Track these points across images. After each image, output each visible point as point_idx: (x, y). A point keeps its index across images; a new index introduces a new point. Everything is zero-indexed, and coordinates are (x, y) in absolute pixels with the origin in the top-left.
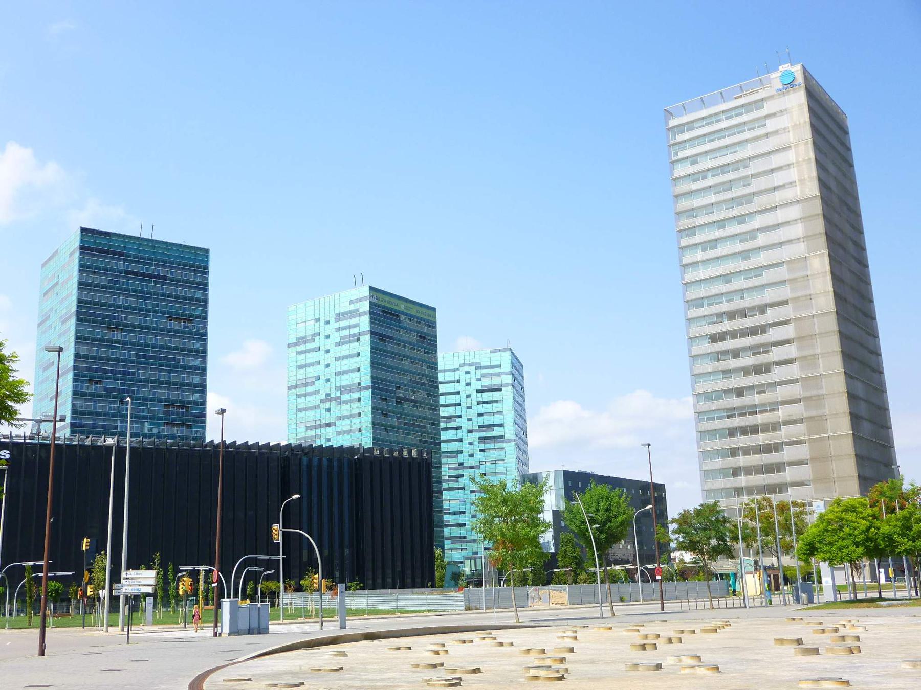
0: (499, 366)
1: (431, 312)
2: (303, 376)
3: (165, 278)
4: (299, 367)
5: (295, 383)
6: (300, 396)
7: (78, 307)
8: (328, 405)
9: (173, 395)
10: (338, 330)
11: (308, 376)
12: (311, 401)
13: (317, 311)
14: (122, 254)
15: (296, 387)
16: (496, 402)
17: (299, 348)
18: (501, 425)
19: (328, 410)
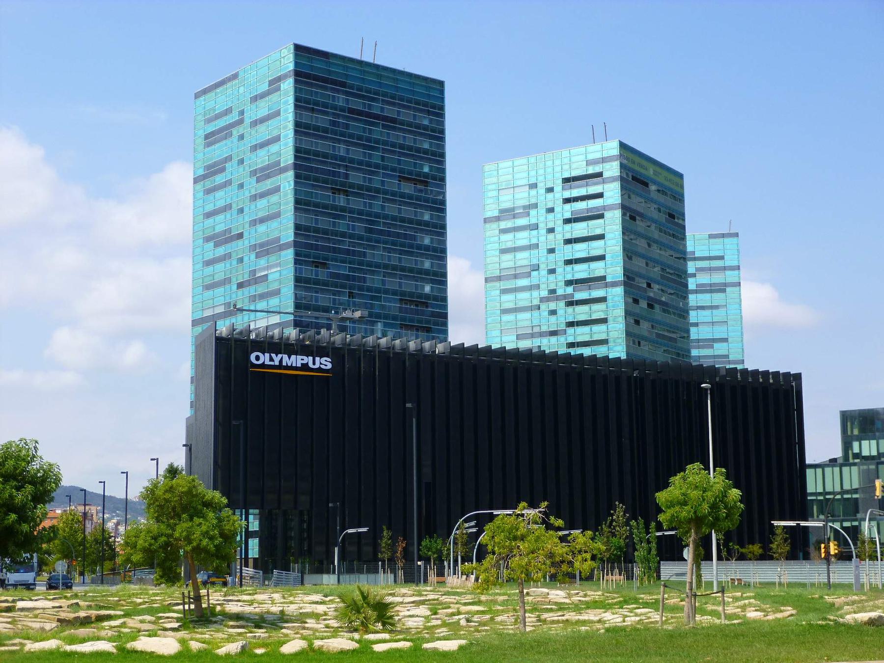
0: (721, 258)
1: (677, 179)
2: (511, 264)
3: (394, 121)
4: (503, 251)
5: (497, 273)
6: (504, 291)
7: (296, 157)
8: (552, 306)
9: (408, 286)
10: (567, 201)
11: (519, 263)
12: (524, 298)
13: (533, 173)
14: (343, 84)
15: (499, 278)
16: (717, 307)
17: (504, 225)
18: (725, 340)
19: (553, 312)
